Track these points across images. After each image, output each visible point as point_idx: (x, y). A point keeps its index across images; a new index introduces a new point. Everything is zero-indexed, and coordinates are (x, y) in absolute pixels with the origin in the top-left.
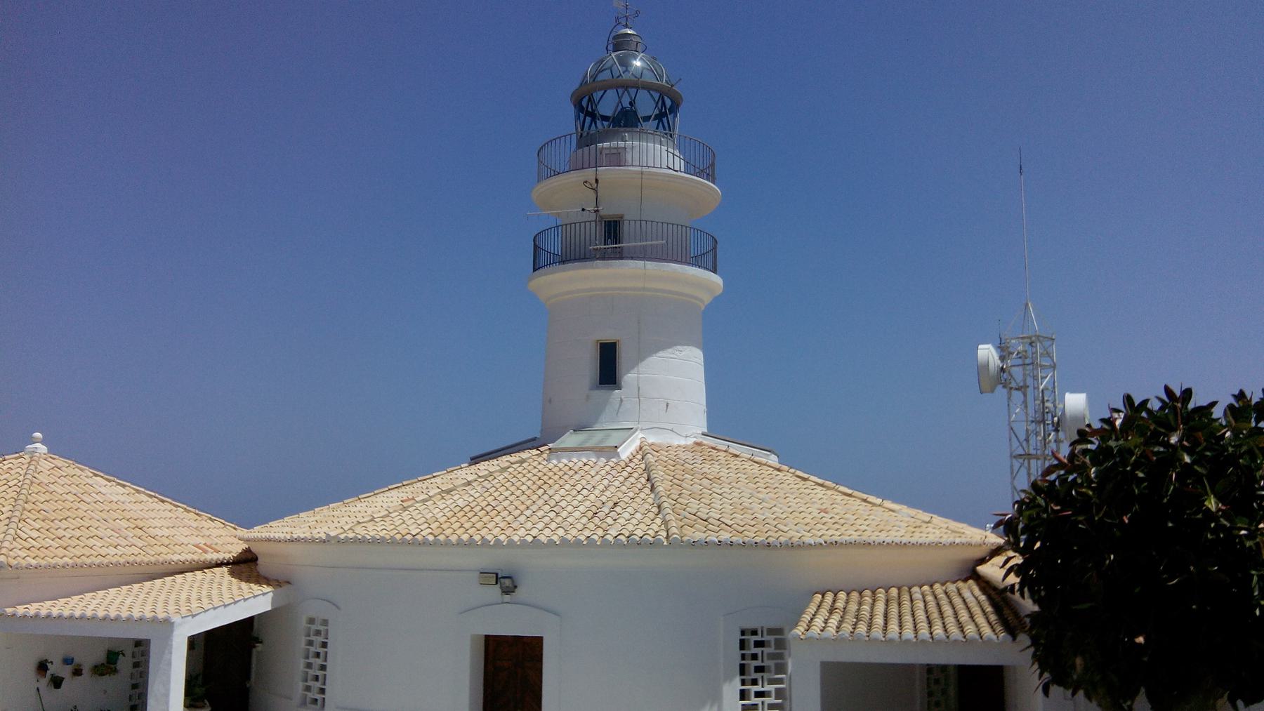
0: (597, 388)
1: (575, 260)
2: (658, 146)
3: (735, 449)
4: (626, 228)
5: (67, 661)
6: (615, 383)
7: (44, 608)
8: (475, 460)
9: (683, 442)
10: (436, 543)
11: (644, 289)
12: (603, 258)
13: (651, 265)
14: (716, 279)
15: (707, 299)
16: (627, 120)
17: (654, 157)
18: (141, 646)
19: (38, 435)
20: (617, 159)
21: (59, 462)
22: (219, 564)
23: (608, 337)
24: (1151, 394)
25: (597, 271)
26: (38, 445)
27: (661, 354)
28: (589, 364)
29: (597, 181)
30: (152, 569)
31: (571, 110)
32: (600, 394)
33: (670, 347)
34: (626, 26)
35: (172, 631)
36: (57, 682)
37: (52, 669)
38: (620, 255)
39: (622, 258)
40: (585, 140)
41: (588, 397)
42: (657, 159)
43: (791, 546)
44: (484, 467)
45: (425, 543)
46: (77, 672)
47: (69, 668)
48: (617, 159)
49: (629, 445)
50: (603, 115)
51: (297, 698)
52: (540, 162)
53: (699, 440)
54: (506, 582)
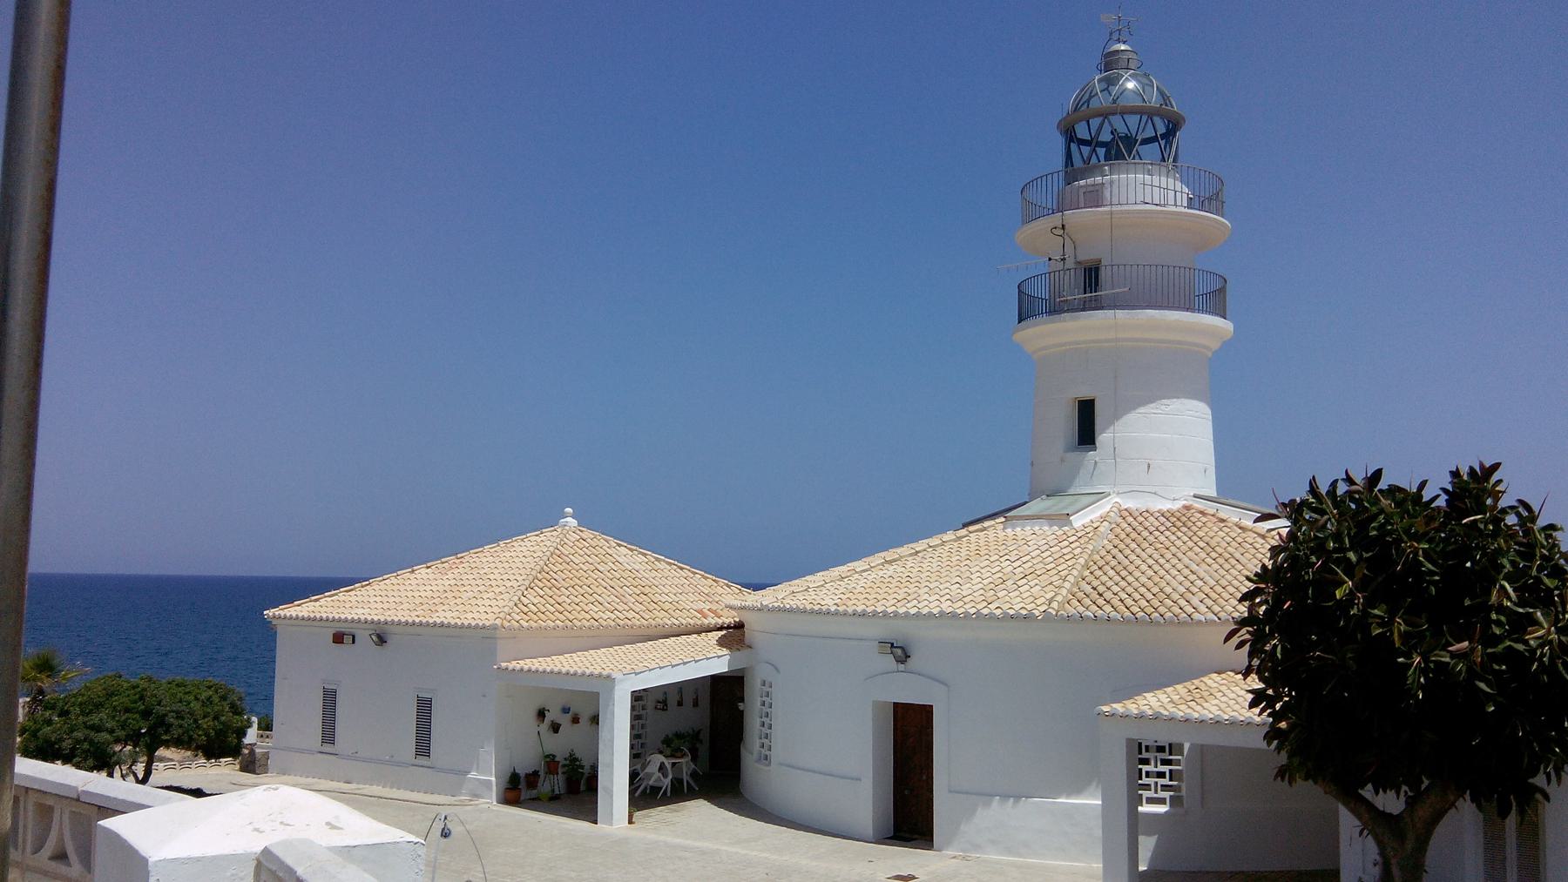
5: (566, 710)
6: (1093, 443)
7: (526, 664)
8: (965, 526)
9: (1166, 506)
10: (837, 613)
11: (1117, 340)
12: (1068, 311)
13: (1121, 314)
14: (1224, 326)
15: (1215, 345)
16: (1120, 149)
17: (1145, 192)
18: (594, 697)
19: (569, 510)
20: (1095, 198)
21: (587, 534)
22: (700, 630)
23: (1086, 394)
24: (1423, 466)
26: (569, 519)
27: (1142, 410)
28: (1065, 422)
30: (649, 632)
31: (1059, 141)
32: (1074, 456)
34: (1119, 41)
35: (613, 688)
36: (555, 728)
37: (549, 717)
38: (1097, 305)
39: (1102, 308)
41: (1062, 460)
43: (1177, 623)
44: (971, 528)
45: (828, 613)
46: (576, 720)
47: (569, 716)
48: (1095, 198)
49: (1093, 512)
50: (1098, 141)
51: (755, 755)
54: (901, 653)
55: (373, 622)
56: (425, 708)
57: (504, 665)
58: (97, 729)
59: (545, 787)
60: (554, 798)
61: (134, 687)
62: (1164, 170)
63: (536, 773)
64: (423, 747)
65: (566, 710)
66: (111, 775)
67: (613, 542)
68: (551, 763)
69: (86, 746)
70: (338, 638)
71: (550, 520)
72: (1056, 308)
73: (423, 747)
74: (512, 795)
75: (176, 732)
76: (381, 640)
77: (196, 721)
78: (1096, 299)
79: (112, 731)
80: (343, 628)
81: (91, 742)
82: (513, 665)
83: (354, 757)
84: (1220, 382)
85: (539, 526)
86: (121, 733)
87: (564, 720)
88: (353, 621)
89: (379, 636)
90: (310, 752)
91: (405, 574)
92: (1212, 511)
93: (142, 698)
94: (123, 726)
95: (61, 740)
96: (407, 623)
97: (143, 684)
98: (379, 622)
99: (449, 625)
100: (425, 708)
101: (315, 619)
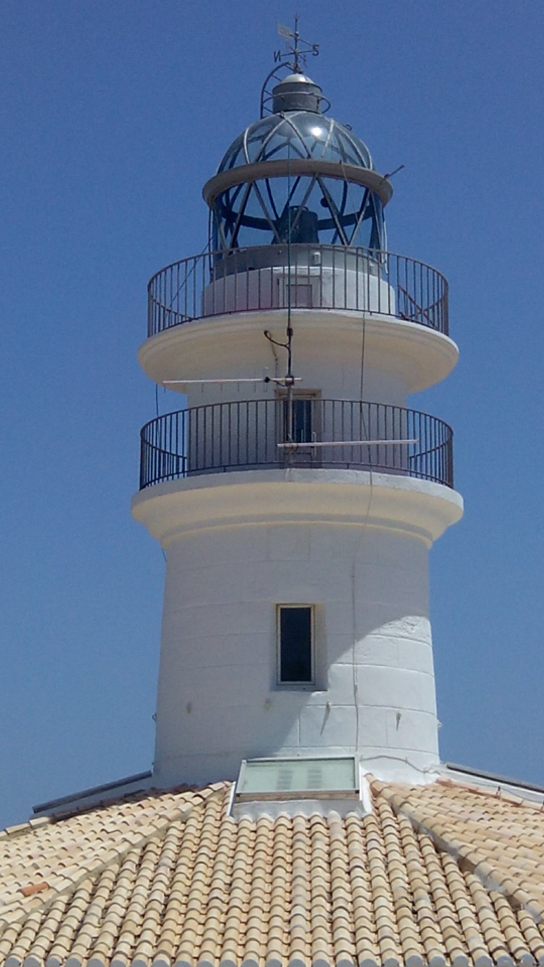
0: (276, 690)
1: (224, 468)
2: (351, 273)
3: (511, 793)
4: (327, 415)
6: (308, 678)
11: (366, 519)
12: (299, 465)
13: (380, 479)
14: (452, 499)
16: (298, 230)
17: (357, 293)
20: (305, 293)
23: (296, 599)
25: (290, 486)
29: (290, 332)
31: (203, 213)
32: (289, 697)
33: (398, 618)
34: (296, 70)
38: (314, 461)
39: (319, 466)
40: (227, 261)
41: (268, 701)
42: (351, 295)
48: (305, 293)
50: (266, 222)
52: (150, 297)
53: (444, 778)
62: (352, 259)
72: (212, 459)
78: (308, 452)
84: (455, 591)
92: (494, 792)
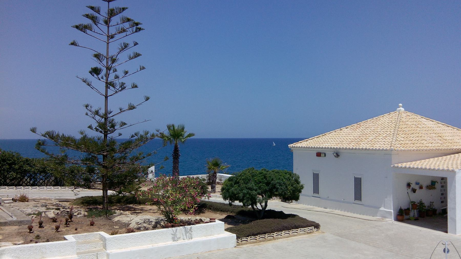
18: (444, 179)
19: (401, 105)
21: (409, 114)
36: (414, 191)
55: (334, 148)
56: (358, 182)
57: (396, 165)
58: (251, 189)
59: (412, 214)
60: (416, 219)
61: (261, 173)
63: (408, 209)
64: (358, 196)
65: (417, 184)
66: (63, 135)
67: (419, 117)
68: (413, 204)
69: (248, 196)
70: (319, 155)
71: (393, 109)
73: (358, 196)
74: (400, 218)
75: (280, 191)
76: (337, 155)
77: (286, 187)
79: (256, 190)
80: (320, 151)
81: (250, 194)
82: (400, 165)
83: (327, 199)
85: (389, 112)
86: (260, 191)
87: (417, 187)
88: (325, 148)
89: (337, 154)
90: (308, 196)
91: (338, 131)
93: (265, 177)
94: (260, 188)
95: (238, 193)
96: (312, 147)
97: (264, 172)
98: (337, 148)
99: (369, 149)
100: (358, 182)
101: (309, 148)
